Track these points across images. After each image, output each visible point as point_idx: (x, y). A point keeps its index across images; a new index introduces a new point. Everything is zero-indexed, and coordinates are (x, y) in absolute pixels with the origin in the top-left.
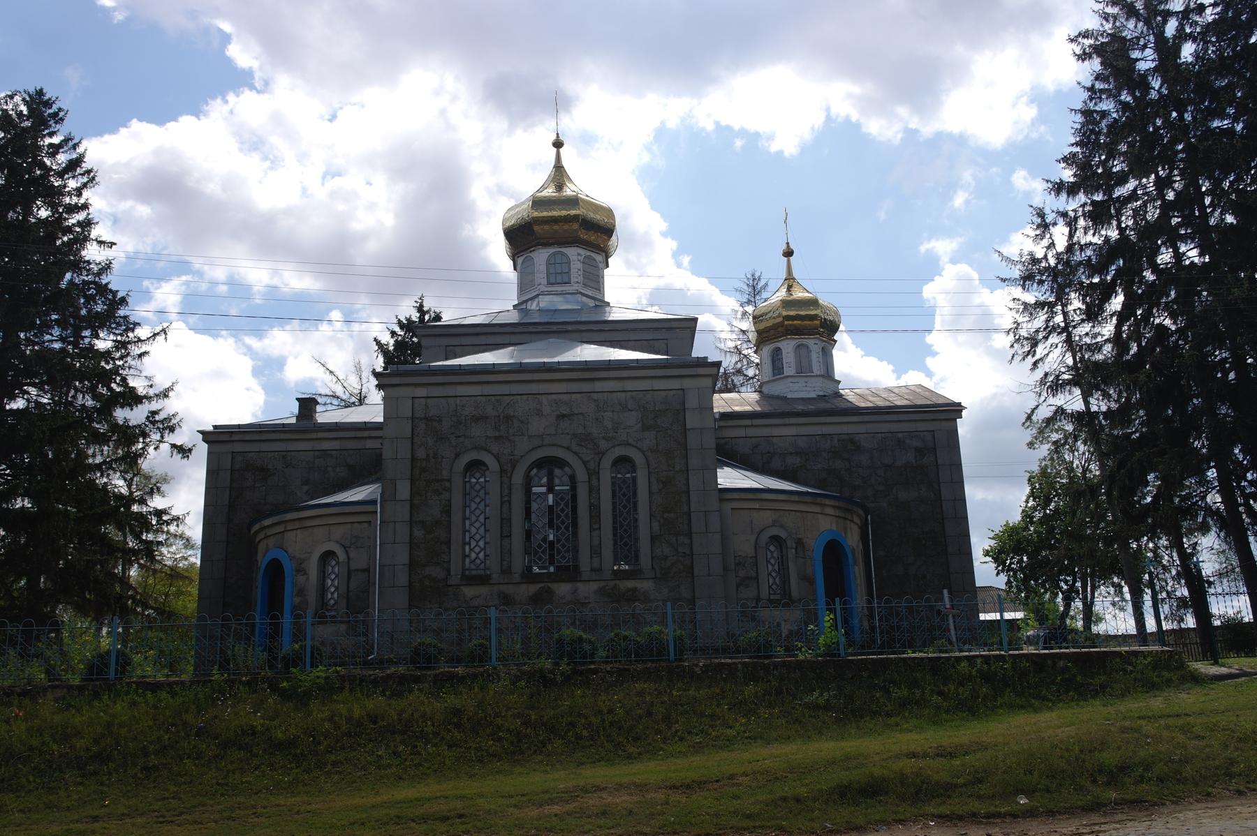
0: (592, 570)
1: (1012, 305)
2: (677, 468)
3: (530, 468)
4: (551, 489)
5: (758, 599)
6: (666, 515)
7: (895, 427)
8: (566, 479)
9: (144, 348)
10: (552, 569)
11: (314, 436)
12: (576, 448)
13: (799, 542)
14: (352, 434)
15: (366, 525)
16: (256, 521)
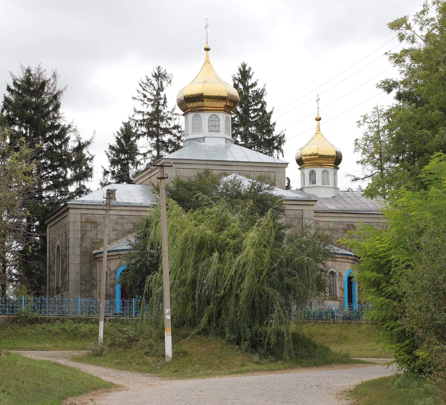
11: (119, 208)
13: (340, 274)
14: (136, 209)
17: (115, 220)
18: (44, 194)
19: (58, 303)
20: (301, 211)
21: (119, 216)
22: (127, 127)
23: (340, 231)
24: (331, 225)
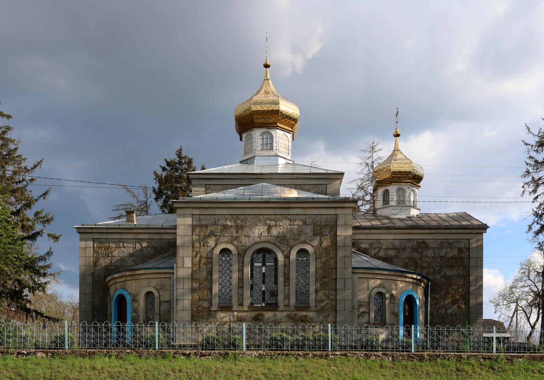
0: (285, 306)
1: (529, 161)
2: (331, 256)
3: (254, 254)
4: (264, 265)
5: (369, 323)
6: (324, 280)
7: (449, 237)
10: (264, 305)
11: (135, 231)
12: (278, 244)
15: (168, 279)
16: (109, 275)
18: (169, 169)
19: (89, 331)
20: (335, 216)
23: (408, 250)
24: (397, 243)
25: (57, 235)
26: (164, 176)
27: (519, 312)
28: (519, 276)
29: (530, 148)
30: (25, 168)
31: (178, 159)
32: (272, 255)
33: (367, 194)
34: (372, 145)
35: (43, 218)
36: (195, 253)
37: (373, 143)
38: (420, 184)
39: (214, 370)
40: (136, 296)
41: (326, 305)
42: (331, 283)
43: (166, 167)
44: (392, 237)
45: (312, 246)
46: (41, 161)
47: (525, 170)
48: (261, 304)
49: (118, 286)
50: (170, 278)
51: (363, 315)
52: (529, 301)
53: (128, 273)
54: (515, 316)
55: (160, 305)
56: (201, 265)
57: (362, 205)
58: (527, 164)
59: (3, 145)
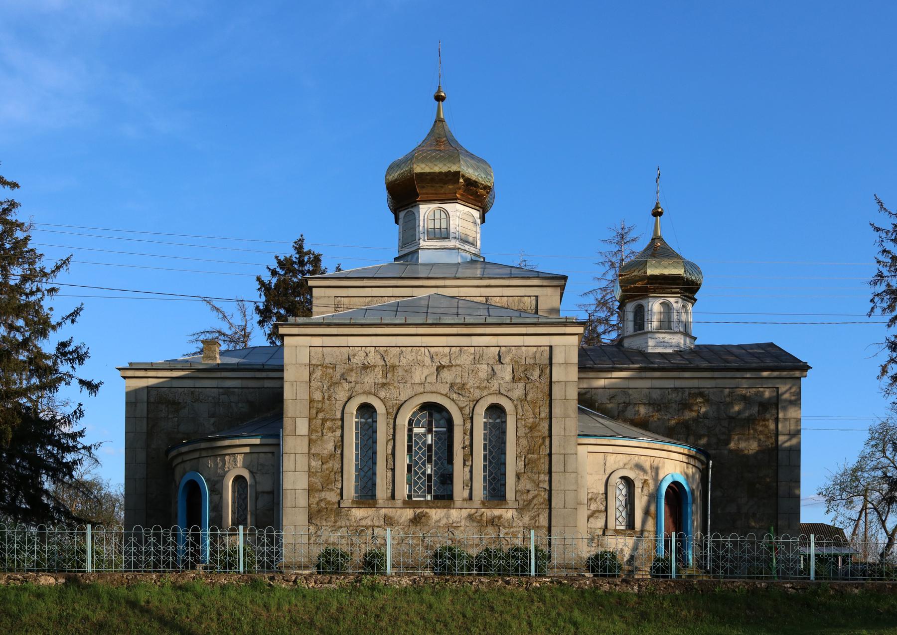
1: (881, 258)
4: (430, 431)
6: (530, 456)
8: (442, 422)
9: (52, 283)
10: (429, 498)
11: (218, 375)
12: (455, 396)
15: (270, 455)
16: (173, 448)
17: (214, 398)
19: (146, 541)
21: (221, 390)
22: (700, 273)
24: (656, 395)
25: (95, 382)
26: (273, 285)
27: (868, 511)
28: (868, 450)
29: (884, 235)
30: (42, 270)
31: (297, 256)
32: (444, 414)
33: (612, 314)
34: (620, 231)
35: (71, 353)
36: (315, 412)
37: (623, 229)
38: (696, 296)
39: (335, 607)
40: (217, 482)
41: (534, 497)
42: (542, 461)
43: (278, 269)
44: (647, 384)
45: (510, 399)
46: (67, 259)
47: (876, 272)
48: (425, 496)
49: (188, 465)
50: (273, 453)
51: (597, 515)
52: (884, 493)
53: (203, 445)
54: (863, 518)
55: (257, 499)
56: (325, 431)
57: (604, 333)
58: (879, 262)
59: (4, 232)
